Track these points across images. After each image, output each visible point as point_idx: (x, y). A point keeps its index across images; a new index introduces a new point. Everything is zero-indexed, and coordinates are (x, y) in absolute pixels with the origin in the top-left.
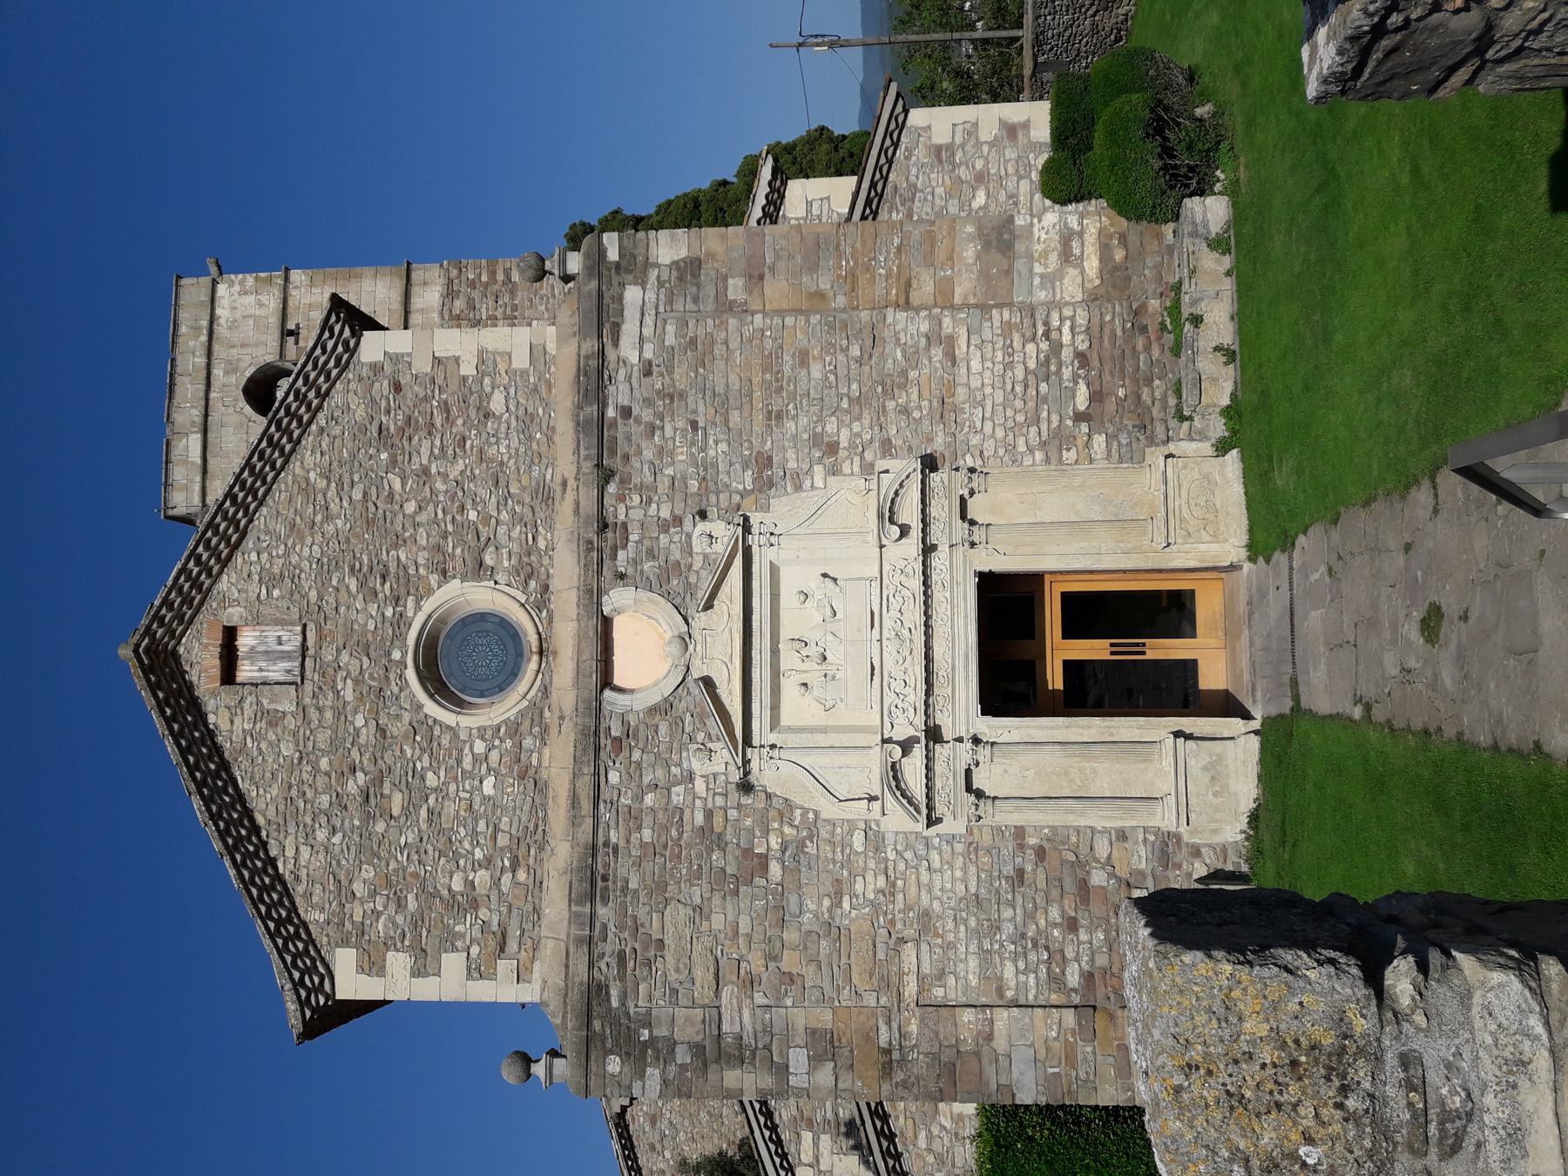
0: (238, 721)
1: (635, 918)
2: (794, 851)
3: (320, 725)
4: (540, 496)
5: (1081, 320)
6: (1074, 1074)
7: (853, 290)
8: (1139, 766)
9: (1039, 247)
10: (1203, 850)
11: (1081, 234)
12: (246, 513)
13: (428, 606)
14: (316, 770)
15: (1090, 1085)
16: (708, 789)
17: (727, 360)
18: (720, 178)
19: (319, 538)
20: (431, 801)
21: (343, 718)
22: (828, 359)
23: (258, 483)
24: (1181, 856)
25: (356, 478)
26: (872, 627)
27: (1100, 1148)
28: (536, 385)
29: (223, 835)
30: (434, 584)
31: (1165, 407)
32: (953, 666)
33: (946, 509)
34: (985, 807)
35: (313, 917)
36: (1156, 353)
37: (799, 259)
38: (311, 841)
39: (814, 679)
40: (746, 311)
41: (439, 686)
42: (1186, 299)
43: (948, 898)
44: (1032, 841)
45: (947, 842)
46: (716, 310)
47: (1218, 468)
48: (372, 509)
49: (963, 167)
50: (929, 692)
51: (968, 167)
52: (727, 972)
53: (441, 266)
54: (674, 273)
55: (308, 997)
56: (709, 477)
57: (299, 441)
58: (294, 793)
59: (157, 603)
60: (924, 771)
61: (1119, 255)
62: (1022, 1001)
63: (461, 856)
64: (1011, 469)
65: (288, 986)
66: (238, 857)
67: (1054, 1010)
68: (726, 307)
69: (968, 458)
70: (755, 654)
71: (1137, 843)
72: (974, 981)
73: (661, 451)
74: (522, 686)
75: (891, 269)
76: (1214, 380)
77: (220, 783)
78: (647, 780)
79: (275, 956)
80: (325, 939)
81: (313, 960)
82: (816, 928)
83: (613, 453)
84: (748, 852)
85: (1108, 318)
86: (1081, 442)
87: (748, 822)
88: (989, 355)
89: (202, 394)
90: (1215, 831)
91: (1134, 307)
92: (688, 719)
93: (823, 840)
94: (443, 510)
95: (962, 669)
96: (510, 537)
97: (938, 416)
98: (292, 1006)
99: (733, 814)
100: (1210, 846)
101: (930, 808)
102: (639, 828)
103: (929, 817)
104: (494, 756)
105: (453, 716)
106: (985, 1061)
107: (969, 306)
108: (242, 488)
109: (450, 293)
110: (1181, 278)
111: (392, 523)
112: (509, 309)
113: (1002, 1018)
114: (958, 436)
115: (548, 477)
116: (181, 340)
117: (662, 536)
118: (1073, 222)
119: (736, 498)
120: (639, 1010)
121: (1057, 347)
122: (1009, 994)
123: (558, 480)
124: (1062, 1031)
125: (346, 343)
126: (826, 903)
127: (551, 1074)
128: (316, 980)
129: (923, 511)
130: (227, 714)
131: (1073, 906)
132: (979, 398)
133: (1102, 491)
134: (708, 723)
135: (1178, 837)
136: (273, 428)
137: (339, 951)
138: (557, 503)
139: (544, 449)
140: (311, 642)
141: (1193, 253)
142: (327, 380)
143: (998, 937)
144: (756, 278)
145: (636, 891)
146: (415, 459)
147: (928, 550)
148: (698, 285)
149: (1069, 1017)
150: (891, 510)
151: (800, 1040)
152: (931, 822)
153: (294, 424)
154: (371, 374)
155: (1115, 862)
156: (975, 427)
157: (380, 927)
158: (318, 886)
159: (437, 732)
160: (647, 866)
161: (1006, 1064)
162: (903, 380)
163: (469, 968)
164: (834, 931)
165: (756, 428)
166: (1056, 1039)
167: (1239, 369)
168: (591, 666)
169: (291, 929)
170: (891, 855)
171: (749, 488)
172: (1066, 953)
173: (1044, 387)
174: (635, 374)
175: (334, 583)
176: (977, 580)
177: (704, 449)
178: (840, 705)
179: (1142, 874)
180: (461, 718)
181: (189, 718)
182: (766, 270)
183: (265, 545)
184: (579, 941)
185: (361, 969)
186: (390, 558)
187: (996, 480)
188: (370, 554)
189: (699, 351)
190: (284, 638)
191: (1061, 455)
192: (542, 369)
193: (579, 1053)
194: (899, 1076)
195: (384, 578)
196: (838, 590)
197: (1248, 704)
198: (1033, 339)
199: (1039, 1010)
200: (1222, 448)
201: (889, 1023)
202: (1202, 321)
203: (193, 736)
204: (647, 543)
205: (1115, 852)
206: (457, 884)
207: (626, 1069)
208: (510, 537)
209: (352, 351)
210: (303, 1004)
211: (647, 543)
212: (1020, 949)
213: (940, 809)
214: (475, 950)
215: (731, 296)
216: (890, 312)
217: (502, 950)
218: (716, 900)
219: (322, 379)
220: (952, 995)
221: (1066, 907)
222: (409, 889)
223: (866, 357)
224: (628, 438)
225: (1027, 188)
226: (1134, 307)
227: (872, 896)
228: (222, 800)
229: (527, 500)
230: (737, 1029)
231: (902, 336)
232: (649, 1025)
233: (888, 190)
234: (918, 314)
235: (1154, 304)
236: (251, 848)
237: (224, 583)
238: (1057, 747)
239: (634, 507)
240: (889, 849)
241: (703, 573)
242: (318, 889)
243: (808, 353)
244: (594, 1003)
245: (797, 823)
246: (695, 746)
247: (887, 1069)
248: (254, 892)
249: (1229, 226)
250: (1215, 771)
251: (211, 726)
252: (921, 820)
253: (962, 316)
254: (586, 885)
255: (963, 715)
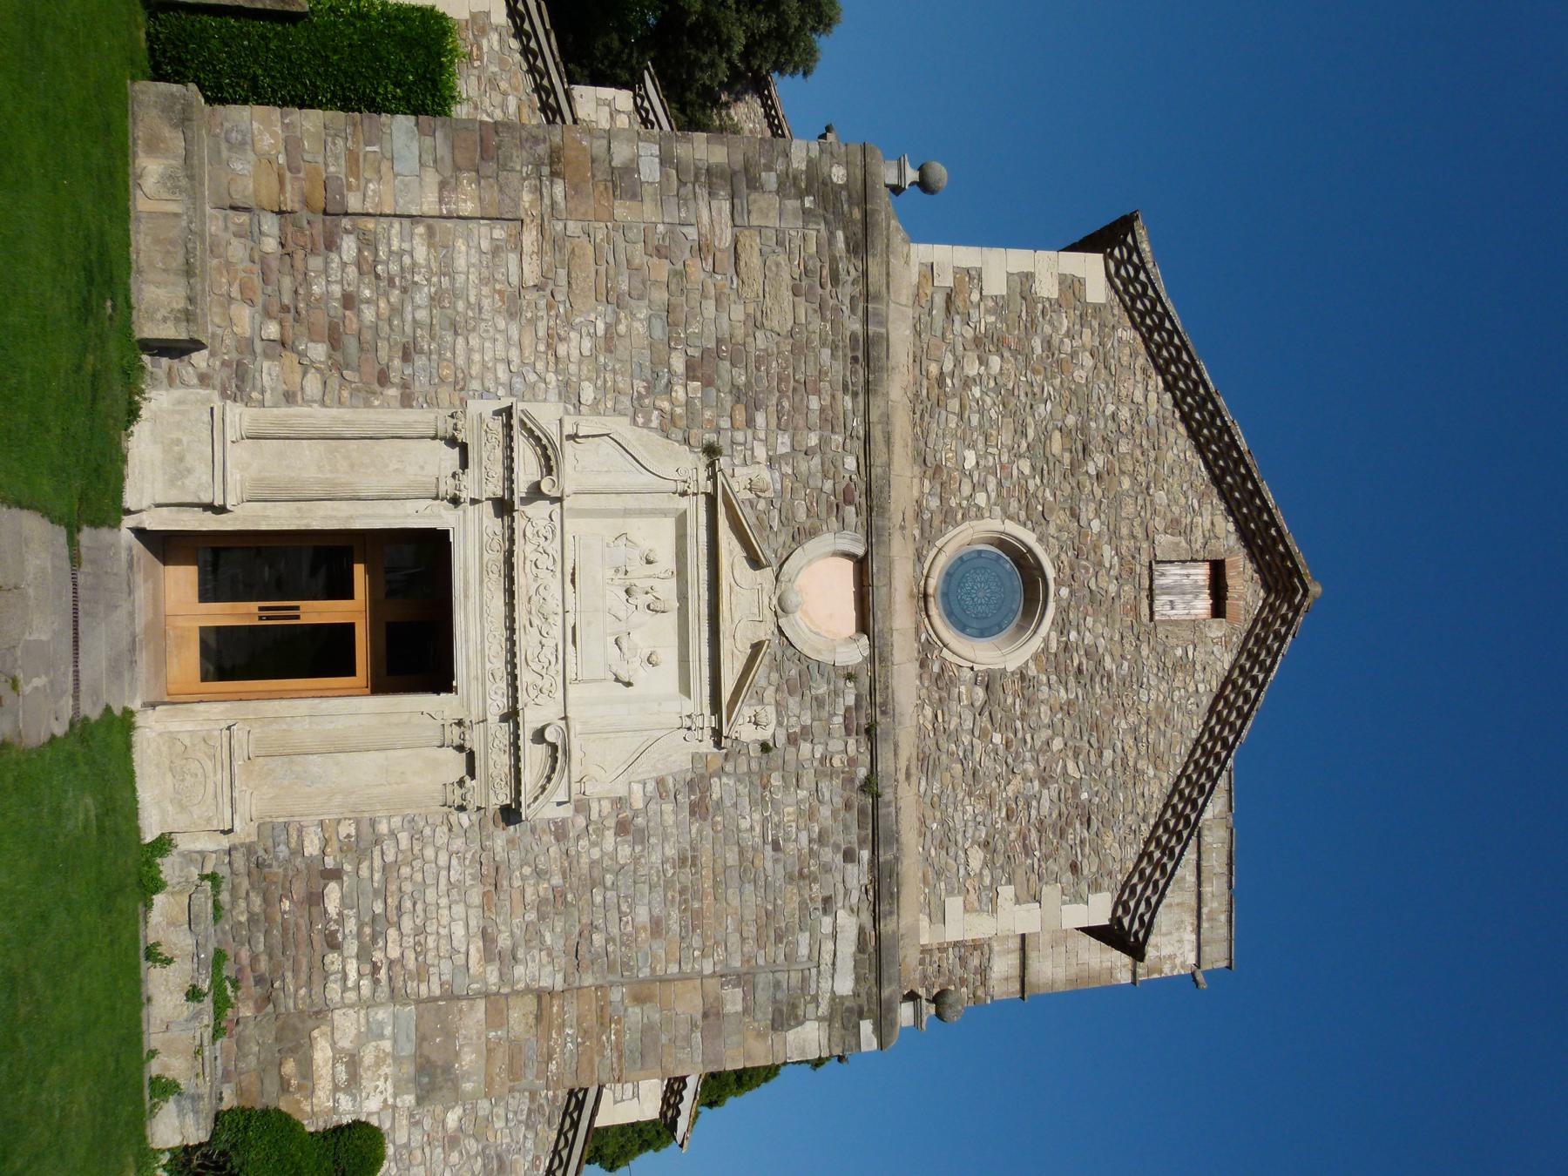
0: (1208, 525)
1: (823, 318)
2: (658, 382)
3: (1132, 520)
4: (931, 763)
5: (334, 989)
6: (349, 144)
7: (602, 1008)
8: (267, 475)
9: (386, 1070)
10: (195, 381)
11: (336, 1088)
12: (1212, 730)
13: (1036, 643)
14: (1133, 476)
15: (332, 132)
16: (752, 449)
17: (742, 920)
18: (716, 1109)
19: (1142, 710)
20: (1024, 445)
21: (1111, 527)
22: (629, 928)
23: (1202, 761)
24: (221, 375)
25: (1110, 772)
26: (574, 628)
27: (321, 70)
28: (939, 879)
29: (1218, 411)
30: (1032, 665)
31: (234, 890)
32: (481, 582)
33: (491, 763)
34: (445, 428)
35: (1128, 334)
36: (245, 954)
37: (664, 1039)
38: (1134, 407)
39: (638, 570)
40: (722, 976)
41: (1022, 561)
42: (207, 1019)
43: (488, 331)
44: (393, 392)
45: (488, 391)
46: (754, 976)
47: (169, 820)
48: (1093, 741)
49: (473, 1152)
50: (509, 555)
51: (468, 1153)
52: (726, 261)
53: (992, 998)
54: (801, 1013)
55: (1130, 256)
56: (760, 790)
57: (1166, 806)
58: (1152, 454)
59: (1290, 638)
60: (515, 465)
61: (289, 1067)
62: (406, 222)
63: (992, 390)
64: (415, 811)
65: (1149, 266)
66: (1201, 390)
67: (371, 211)
68: (745, 979)
69: (466, 823)
70: (705, 595)
71: (273, 390)
72: (460, 245)
73: (811, 815)
74: (942, 562)
75: (559, 1034)
76: (172, 923)
77: (1221, 463)
78: (817, 460)
79: (1163, 295)
80: (1116, 311)
81: (1126, 291)
82: (632, 302)
83: (862, 811)
84: (708, 383)
85: (303, 992)
86: (335, 845)
87: (708, 414)
88: (443, 942)
89: (1204, 856)
90: (180, 402)
91: (271, 1006)
92: (776, 524)
93: (625, 394)
94: (1025, 742)
95: (472, 581)
96: (960, 717)
97: (501, 870)
98: (1145, 246)
99: (725, 423)
100: (185, 384)
101: (508, 426)
102: (822, 410)
103: (510, 416)
104: (967, 489)
105: (1007, 531)
106: (448, 161)
107: (467, 997)
108: (1217, 756)
109: (983, 971)
110: (214, 1044)
111: (1074, 726)
112: (927, 960)
113: (429, 203)
114: (478, 848)
115: (923, 783)
116: (1225, 907)
117: (809, 722)
118: (345, 1102)
119: (729, 767)
120: (815, 227)
121: (363, 955)
122: (421, 230)
123: (914, 779)
124: (362, 188)
125: (1126, 910)
126: (622, 329)
127: (900, 169)
128: (1123, 272)
129: (518, 759)
130: (1217, 530)
131: (347, 322)
132: (454, 892)
133: (308, 789)
134: (754, 519)
135: (224, 395)
136: (1193, 817)
137: (1102, 300)
138: (915, 755)
139: (929, 813)
140: (1145, 603)
141: (197, 1075)
142: (1143, 871)
143: (433, 290)
144: (712, 1014)
145: (823, 345)
146: (1055, 795)
147: (512, 716)
148: (775, 1001)
149: (354, 203)
150: (555, 760)
151: (648, 191)
152: (508, 412)
153: (1172, 824)
154: (1100, 880)
155: (298, 369)
156: (459, 858)
157: (1065, 321)
158: (1125, 363)
159: (1023, 515)
160: (812, 371)
161: (425, 157)
162: (544, 908)
163: (980, 279)
164: (612, 299)
165: (709, 846)
166: (368, 181)
167: (141, 937)
168: (878, 581)
169: (1148, 321)
170: (551, 377)
171: (716, 779)
172: (356, 270)
173: (378, 908)
174: (840, 898)
175: (1126, 664)
176: (454, 684)
177: (765, 820)
178: (610, 540)
179: (266, 356)
180: (1001, 528)
181: (1252, 526)
182: (700, 1023)
183: (1192, 700)
184: (878, 298)
185: (1082, 282)
186: (1075, 691)
187: (433, 798)
188: (1094, 694)
189: (772, 929)
190: (1168, 607)
191: (357, 829)
192: (932, 898)
193: (874, 187)
194: (542, 150)
195: (1080, 671)
196: (614, 669)
197: (138, 546)
198: (391, 963)
199: (388, 212)
200: (163, 844)
201: (553, 204)
202: (187, 994)
203: (1248, 508)
204: (825, 714)
205: (298, 379)
206: (995, 361)
207: (826, 170)
208: (960, 717)
209: (1119, 902)
210: (1135, 249)
211: (825, 714)
212: (409, 277)
213: (497, 425)
214: (975, 297)
215: (739, 992)
216: (559, 986)
217: (949, 297)
218: (740, 333)
219: (1148, 872)
220: (484, 230)
221: (355, 320)
222: (1040, 358)
223: (586, 933)
224: (846, 828)
225: (399, 1135)
226: (271, 1006)
227: (573, 335)
228: (1218, 447)
229: (944, 757)
230: (714, 203)
231: (545, 959)
232: (805, 211)
233: (558, 1121)
234: (527, 985)
235: (246, 1011)
236: (1189, 400)
237: (1228, 660)
238: (362, 494)
239: (838, 753)
240: (554, 383)
241: (763, 683)
242: (1125, 360)
243: (652, 933)
244: (860, 236)
245: (656, 412)
246: (767, 494)
247: (555, 156)
248: (1185, 357)
249: (151, 1111)
250: (178, 467)
251: (1231, 519)
252: (519, 413)
253: (475, 986)
254: (873, 353)
255: (470, 528)
